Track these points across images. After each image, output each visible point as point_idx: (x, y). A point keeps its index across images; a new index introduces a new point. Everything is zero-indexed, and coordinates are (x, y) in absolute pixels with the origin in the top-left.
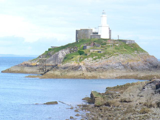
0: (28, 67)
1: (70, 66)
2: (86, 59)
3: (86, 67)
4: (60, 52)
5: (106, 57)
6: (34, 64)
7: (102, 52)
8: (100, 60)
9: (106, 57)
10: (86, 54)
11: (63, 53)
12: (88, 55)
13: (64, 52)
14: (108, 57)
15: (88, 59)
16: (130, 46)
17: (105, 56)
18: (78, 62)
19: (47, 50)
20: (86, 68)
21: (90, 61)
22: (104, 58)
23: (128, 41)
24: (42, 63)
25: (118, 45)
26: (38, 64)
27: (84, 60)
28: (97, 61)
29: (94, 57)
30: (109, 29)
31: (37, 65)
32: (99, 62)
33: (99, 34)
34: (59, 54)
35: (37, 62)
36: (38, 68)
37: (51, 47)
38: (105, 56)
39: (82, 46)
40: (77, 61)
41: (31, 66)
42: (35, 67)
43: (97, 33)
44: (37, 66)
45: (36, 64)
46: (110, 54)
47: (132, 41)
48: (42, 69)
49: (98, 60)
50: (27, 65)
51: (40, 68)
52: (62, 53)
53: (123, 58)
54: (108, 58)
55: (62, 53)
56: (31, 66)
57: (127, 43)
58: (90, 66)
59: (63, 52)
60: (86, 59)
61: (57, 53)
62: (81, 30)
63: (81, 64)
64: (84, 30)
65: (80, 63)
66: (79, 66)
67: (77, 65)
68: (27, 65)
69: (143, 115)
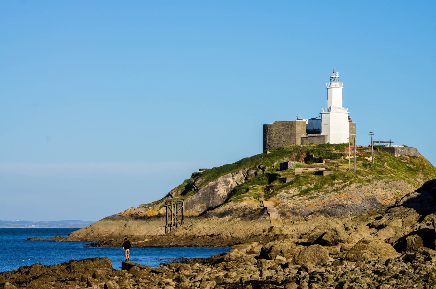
0: (138, 222)
1: (237, 210)
2: (284, 191)
3: (280, 210)
4: (220, 179)
5: (337, 187)
6: (152, 212)
7: (326, 173)
8: (320, 194)
9: (336, 185)
10: (284, 180)
11: (229, 182)
12: (288, 181)
13: (230, 179)
14: (343, 185)
15: (287, 192)
16: (405, 161)
17: (334, 184)
18: (262, 199)
19: (189, 177)
20: (279, 213)
21: (294, 198)
22: (330, 189)
23: (400, 150)
24: (173, 211)
25: (371, 158)
26: (162, 211)
27: (278, 195)
28: (311, 198)
29: (304, 188)
30: (350, 120)
31: (159, 216)
32: (317, 199)
33: (322, 134)
34: (218, 186)
35: (161, 207)
36: (162, 222)
37: (200, 170)
38: (334, 184)
39: (277, 163)
40: (257, 197)
41: (145, 218)
42: (156, 222)
43: (319, 132)
44: (161, 218)
45: (157, 213)
46: (348, 178)
47: (409, 149)
48: (174, 225)
49: (315, 193)
50: (136, 217)
51: (169, 222)
52: (227, 183)
53: (383, 188)
54: (343, 188)
55: (227, 183)
56: (145, 218)
57: (396, 155)
58: (293, 208)
59: (228, 179)
60: (282, 193)
61: (211, 183)
62: (276, 123)
63: (268, 204)
64: (283, 123)
65: (265, 202)
66: (262, 208)
67: (256, 205)
68: (136, 217)
69: (389, 168)
